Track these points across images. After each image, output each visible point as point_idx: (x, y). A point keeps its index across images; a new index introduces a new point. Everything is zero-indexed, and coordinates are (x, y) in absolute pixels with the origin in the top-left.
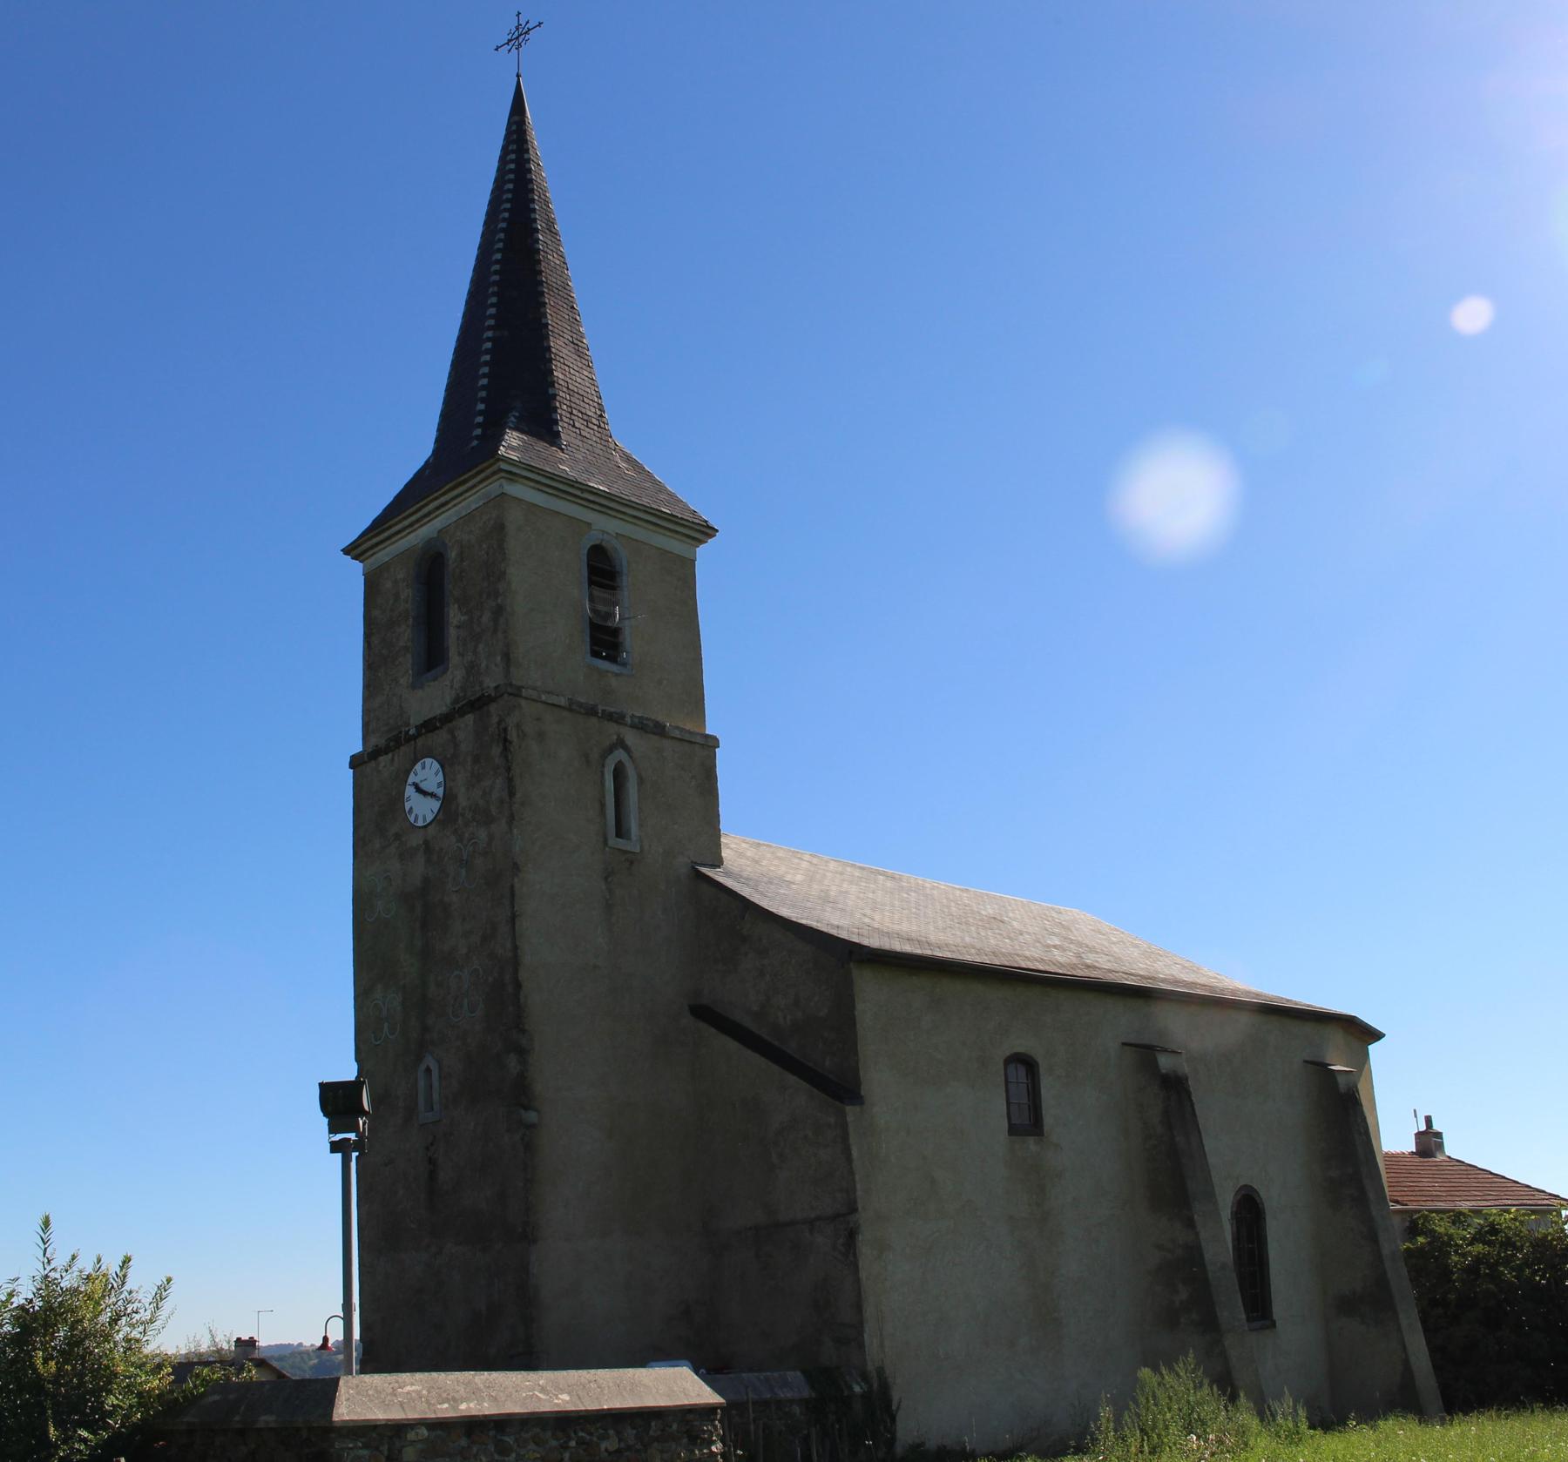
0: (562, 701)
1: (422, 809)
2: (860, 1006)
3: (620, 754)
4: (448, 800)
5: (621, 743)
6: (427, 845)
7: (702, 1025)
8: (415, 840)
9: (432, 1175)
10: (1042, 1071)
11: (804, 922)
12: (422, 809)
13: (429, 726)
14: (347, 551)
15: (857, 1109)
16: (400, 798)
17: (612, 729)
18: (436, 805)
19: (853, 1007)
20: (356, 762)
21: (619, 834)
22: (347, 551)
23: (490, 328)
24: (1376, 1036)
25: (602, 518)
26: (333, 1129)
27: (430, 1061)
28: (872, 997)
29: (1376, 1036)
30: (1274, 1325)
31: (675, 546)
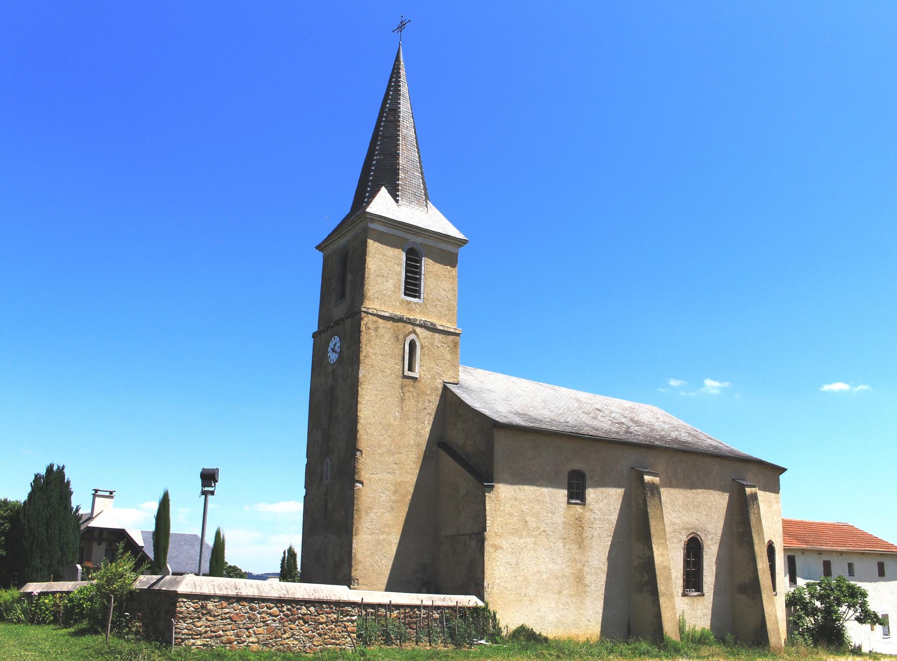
0: (387, 315)
1: (333, 357)
2: (496, 447)
3: (413, 336)
4: (341, 354)
5: (414, 332)
6: (334, 372)
7: (441, 451)
8: (330, 369)
9: (326, 505)
10: (587, 477)
11: (480, 410)
12: (333, 357)
13: (337, 323)
14: (317, 248)
15: (771, 496)
16: (327, 352)
17: (410, 327)
18: (337, 356)
19: (493, 447)
20: (314, 335)
21: (411, 369)
22: (317, 248)
23: (377, 155)
24: (783, 470)
25: (414, 237)
26: (203, 486)
27: (328, 460)
28: (501, 444)
29: (783, 470)
30: (703, 595)
31: (450, 248)
